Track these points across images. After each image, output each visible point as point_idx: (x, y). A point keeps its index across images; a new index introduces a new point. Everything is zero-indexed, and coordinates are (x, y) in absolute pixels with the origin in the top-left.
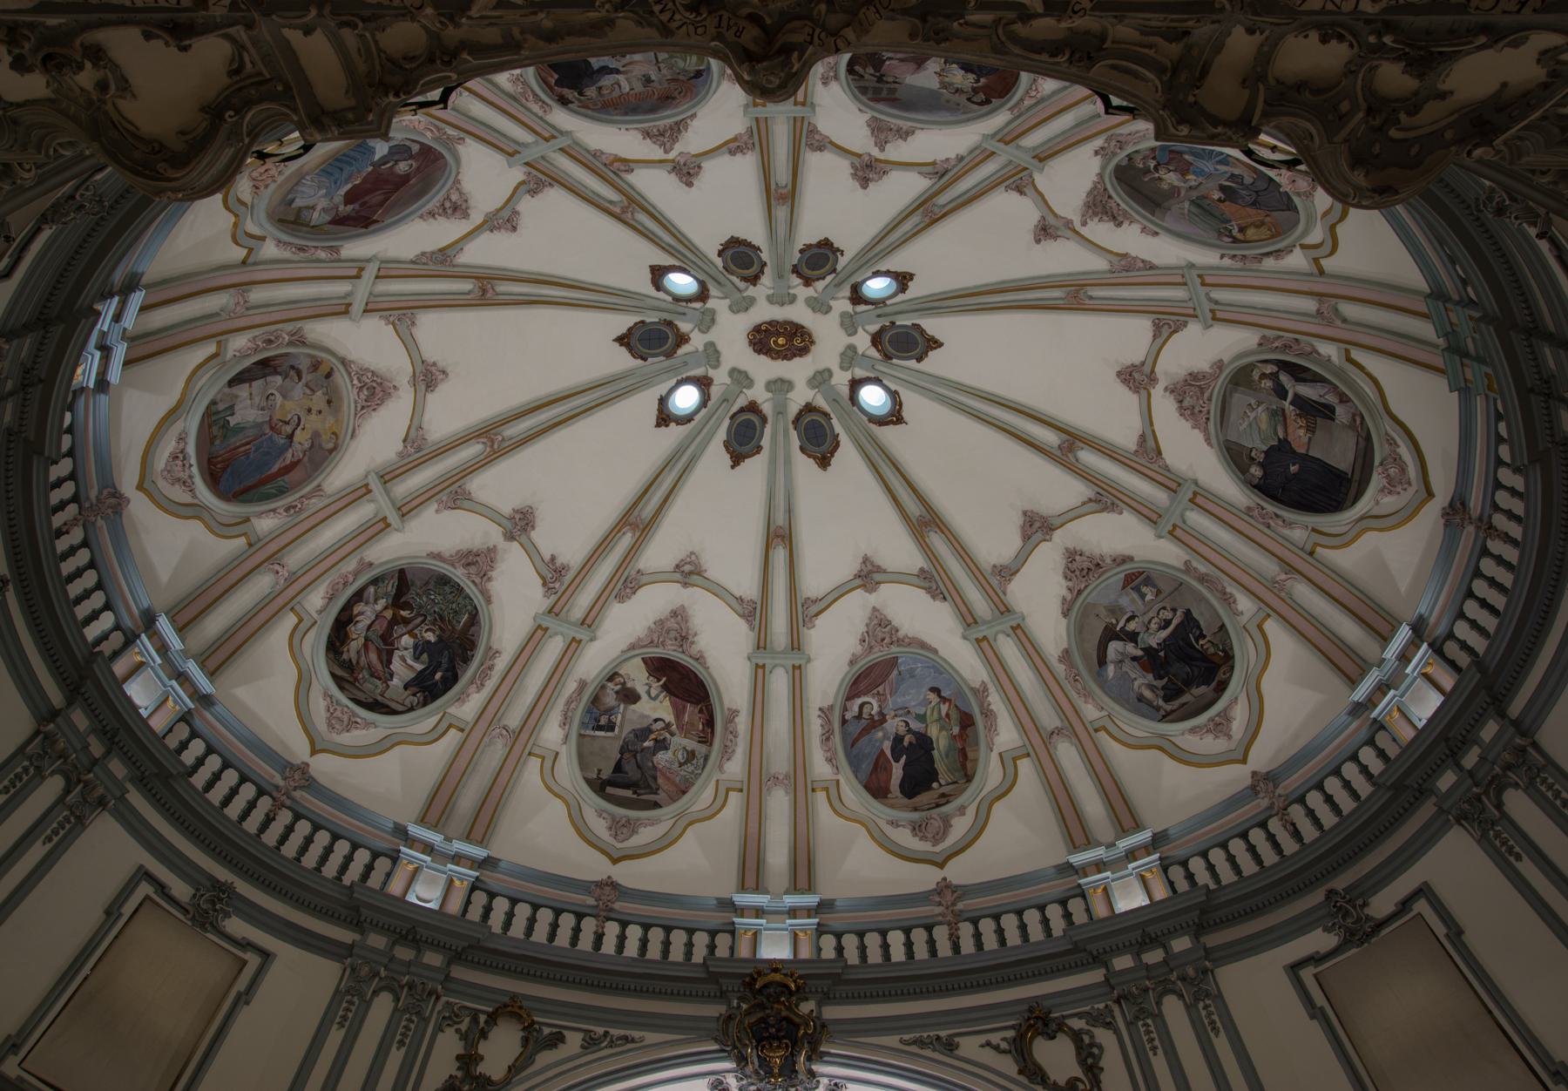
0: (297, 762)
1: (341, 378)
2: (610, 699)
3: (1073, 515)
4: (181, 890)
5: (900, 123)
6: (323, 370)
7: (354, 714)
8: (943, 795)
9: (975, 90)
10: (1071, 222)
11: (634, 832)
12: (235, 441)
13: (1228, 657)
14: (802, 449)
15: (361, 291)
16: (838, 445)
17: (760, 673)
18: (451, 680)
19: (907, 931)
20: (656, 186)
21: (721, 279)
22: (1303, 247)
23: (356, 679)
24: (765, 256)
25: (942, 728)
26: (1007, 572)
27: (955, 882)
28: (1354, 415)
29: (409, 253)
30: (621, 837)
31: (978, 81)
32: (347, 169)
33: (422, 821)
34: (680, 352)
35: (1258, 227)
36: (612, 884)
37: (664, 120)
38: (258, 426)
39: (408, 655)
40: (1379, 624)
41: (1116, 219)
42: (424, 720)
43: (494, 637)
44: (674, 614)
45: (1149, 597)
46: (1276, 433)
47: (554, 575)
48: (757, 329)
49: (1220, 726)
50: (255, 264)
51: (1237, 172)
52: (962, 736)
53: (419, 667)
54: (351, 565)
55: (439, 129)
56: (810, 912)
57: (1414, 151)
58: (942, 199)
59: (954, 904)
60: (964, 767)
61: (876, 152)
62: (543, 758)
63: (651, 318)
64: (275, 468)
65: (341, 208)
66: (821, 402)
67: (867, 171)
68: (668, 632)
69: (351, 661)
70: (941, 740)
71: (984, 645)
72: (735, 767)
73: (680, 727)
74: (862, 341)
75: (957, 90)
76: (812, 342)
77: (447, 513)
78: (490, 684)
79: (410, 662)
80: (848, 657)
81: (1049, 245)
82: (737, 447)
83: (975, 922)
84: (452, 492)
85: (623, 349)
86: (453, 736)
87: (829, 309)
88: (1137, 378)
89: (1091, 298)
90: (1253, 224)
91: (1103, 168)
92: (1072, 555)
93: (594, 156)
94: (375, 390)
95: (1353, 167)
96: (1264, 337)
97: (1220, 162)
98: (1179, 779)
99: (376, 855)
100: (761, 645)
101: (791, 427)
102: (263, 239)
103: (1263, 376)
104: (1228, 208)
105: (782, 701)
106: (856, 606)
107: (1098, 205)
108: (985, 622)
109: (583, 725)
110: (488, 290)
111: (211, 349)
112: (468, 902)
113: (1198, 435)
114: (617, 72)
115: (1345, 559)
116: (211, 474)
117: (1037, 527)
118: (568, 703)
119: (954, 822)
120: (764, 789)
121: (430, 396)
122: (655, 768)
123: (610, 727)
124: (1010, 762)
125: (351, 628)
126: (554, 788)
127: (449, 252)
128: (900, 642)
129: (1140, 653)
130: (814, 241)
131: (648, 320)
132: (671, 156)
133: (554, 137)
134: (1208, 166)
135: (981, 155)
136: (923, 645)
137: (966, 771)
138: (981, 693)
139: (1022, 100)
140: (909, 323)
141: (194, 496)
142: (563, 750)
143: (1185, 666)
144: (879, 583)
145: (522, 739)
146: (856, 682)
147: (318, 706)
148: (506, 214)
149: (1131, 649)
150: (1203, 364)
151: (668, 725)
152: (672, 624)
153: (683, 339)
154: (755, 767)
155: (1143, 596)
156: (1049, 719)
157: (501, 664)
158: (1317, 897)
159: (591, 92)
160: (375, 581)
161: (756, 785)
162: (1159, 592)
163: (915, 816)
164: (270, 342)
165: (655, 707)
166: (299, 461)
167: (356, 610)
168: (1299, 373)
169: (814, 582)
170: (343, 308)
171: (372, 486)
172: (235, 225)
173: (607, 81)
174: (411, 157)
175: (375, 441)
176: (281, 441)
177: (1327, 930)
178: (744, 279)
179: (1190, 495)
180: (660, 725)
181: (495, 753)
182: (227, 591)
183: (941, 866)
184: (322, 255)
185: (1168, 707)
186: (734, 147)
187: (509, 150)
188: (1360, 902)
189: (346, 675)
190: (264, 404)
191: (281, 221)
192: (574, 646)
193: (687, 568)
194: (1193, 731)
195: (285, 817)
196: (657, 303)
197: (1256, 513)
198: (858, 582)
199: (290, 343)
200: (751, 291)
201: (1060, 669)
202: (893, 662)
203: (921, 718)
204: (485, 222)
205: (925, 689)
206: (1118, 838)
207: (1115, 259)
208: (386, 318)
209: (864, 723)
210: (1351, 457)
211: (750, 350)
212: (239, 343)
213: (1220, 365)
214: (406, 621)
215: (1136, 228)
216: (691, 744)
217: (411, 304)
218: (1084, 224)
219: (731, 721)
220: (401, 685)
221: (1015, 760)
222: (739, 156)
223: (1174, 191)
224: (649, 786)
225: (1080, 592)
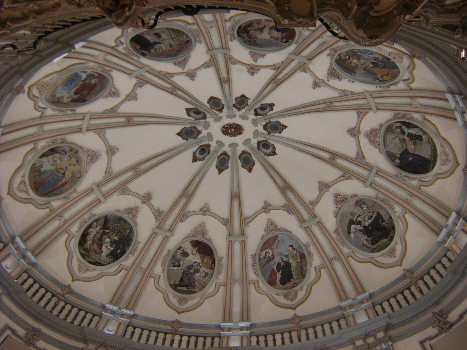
0: (66, 284)
1: (81, 153)
2: (179, 256)
3: (336, 182)
4: (21, 332)
5: (260, 52)
6: (74, 151)
7: (88, 267)
8: (295, 283)
9: (283, 38)
10: (324, 80)
11: (186, 302)
12: (43, 176)
13: (393, 228)
14: (242, 166)
15: (85, 124)
16: (254, 164)
17: (230, 244)
18: (123, 252)
19: (282, 334)
20: (182, 81)
21: (210, 111)
22: (403, 80)
23: (89, 254)
24: (223, 102)
25: (294, 259)
26: (314, 203)
27: (299, 315)
28: (429, 138)
29: (101, 110)
30: (182, 304)
31: (282, 35)
32: (73, 83)
33: (111, 303)
34: (199, 136)
35: (387, 75)
36: (178, 322)
37: (180, 58)
38: (51, 171)
39: (108, 245)
40: (446, 214)
41: (338, 77)
42: (113, 267)
43: (139, 236)
44: (200, 225)
45: (364, 208)
46: (403, 147)
47: (159, 215)
48: (224, 127)
49: (392, 253)
50: (45, 117)
51: (376, 56)
52: (301, 262)
53: (112, 249)
54: (88, 215)
55: (102, 67)
56: (248, 328)
57: (383, 20)
58: (280, 77)
59: (299, 323)
60: (302, 273)
61: (254, 63)
62: (155, 278)
63: (188, 126)
64: (59, 185)
65: (74, 96)
66: (248, 150)
67: (252, 70)
68: (198, 231)
69: (87, 248)
70: (294, 264)
71: (307, 229)
72: (222, 278)
73: (203, 264)
74: (260, 128)
75: (276, 39)
76: (243, 130)
77: (122, 196)
78: (137, 253)
79: (109, 247)
80: (261, 236)
81: (318, 89)
82: (220, 167)
83: (306, 329)
84: (123, 189)
85: (180, 137)
86: (123, 272)
87: (248, 118)
88: (354, 132)
89: (335, 106)
90: (385, 75)
91: (331, 60)
92: (336, 196)
93: (159, 73)
94: (93, 156)
95: (358, 29)
96: (395, 114)
97: (370, 54)
98: (377, 274)
99: (94, 316)
100: (231, 234)
101: (238, 159)
102: (46, 108)
103: (396, 127)
104: (375, 70)
105: (238, 254)
106: (263, 218)
107: (332, 74)
108: (308, 221)
109: (169, 265)
110: (130, 120)
111: (31, 146)
112: (126, 331)
113: (376, 151)
114: (160, 43)
115: (431, 190)
116: (35, 188)
117: (324, 187)
118: (164, 258)
119: (299, 293)
120: (232, 284)
121: (113, 157)
122: (194, 279)
123: (179, 266)
124: (318, 270)
125: (88, 237)
126: (158, 288)
127: (115, 109)
128: (278, 230)
129: (362, 228)
130: (239, 95)
131: (187, 127)
132: (185, 70)
133: (143, 67)
134: (366, 56)
135: (288, 61)
136: (286, 231)
137: (303, 274)
138: (307, 246)
139: (298, 40)
140: (275, 121)
141: (29, 195)
142: (162, 275)
143: (378, 232)
144: (270, 210)
145: (148, 272)
146: (264, 245)
147: (75, 265)
148: (132, 95)
149: (359, 227)
150: (375, 125)
151: (199, 264)
152: (200, 229)
153: (199, 132)
154: (229, 277)
155: (362, 208)
156: (331, 254)
157: (140, 246)
158: (429, 315)
159: (152, 51)
160: (96, 221)
161: (228, 284)
162: (368, 206)
163: (286, 291)
164: (54, 142)
165: (194, 258)
166: (67, 182)
167: (90, 230)
168: (409, 125)
169: (248, 211)
170: (79, 130)
171: (94, 189)
172: (35, 104)
173: (157, 47)
174: (95, 78)
175: (94, 174)
176: (61, 175)
177: (433, 327)
178: (218, 110)
179: (375, 171)
180: (196, 264)
181: (138, 277)
182: (42, 226)
183: (294, 309)
184: (69, 112)
185: (373, 247)
186: (206, 65)
187: (130, 73)
188: (445, 316)
189: (85, 252)
190: (53, 163)
191: (52, 102)
192: (166, 238)
193: (205, 209)
194: (382, 255)
195: (62, 304)
196: (189, 121)
197: (399, 176)
198: (263, 210)
199: (61, 143)
200: (221, 114)
201: (334, 236)
202: (276, 237)
203: (287, 256)
204: (126, 98)
205: (288, 246)
206: (357, 296)
207: (341, 92)
208: (95, 132)
209: (267, 259)
210: (430, 153)
211: (222, 134)
212: (42, 144)
213: (381, 125)
214: (107, 233)
215: (346, 80)
216: (207, 270)
217: (103, 127)
218: (328, 81)
219: (221, 261)
220: (105, 255)
221: (320, 269)
222: (208, 69)
223: (356, 66)
224: (192, 286)
225: (340, 208)
